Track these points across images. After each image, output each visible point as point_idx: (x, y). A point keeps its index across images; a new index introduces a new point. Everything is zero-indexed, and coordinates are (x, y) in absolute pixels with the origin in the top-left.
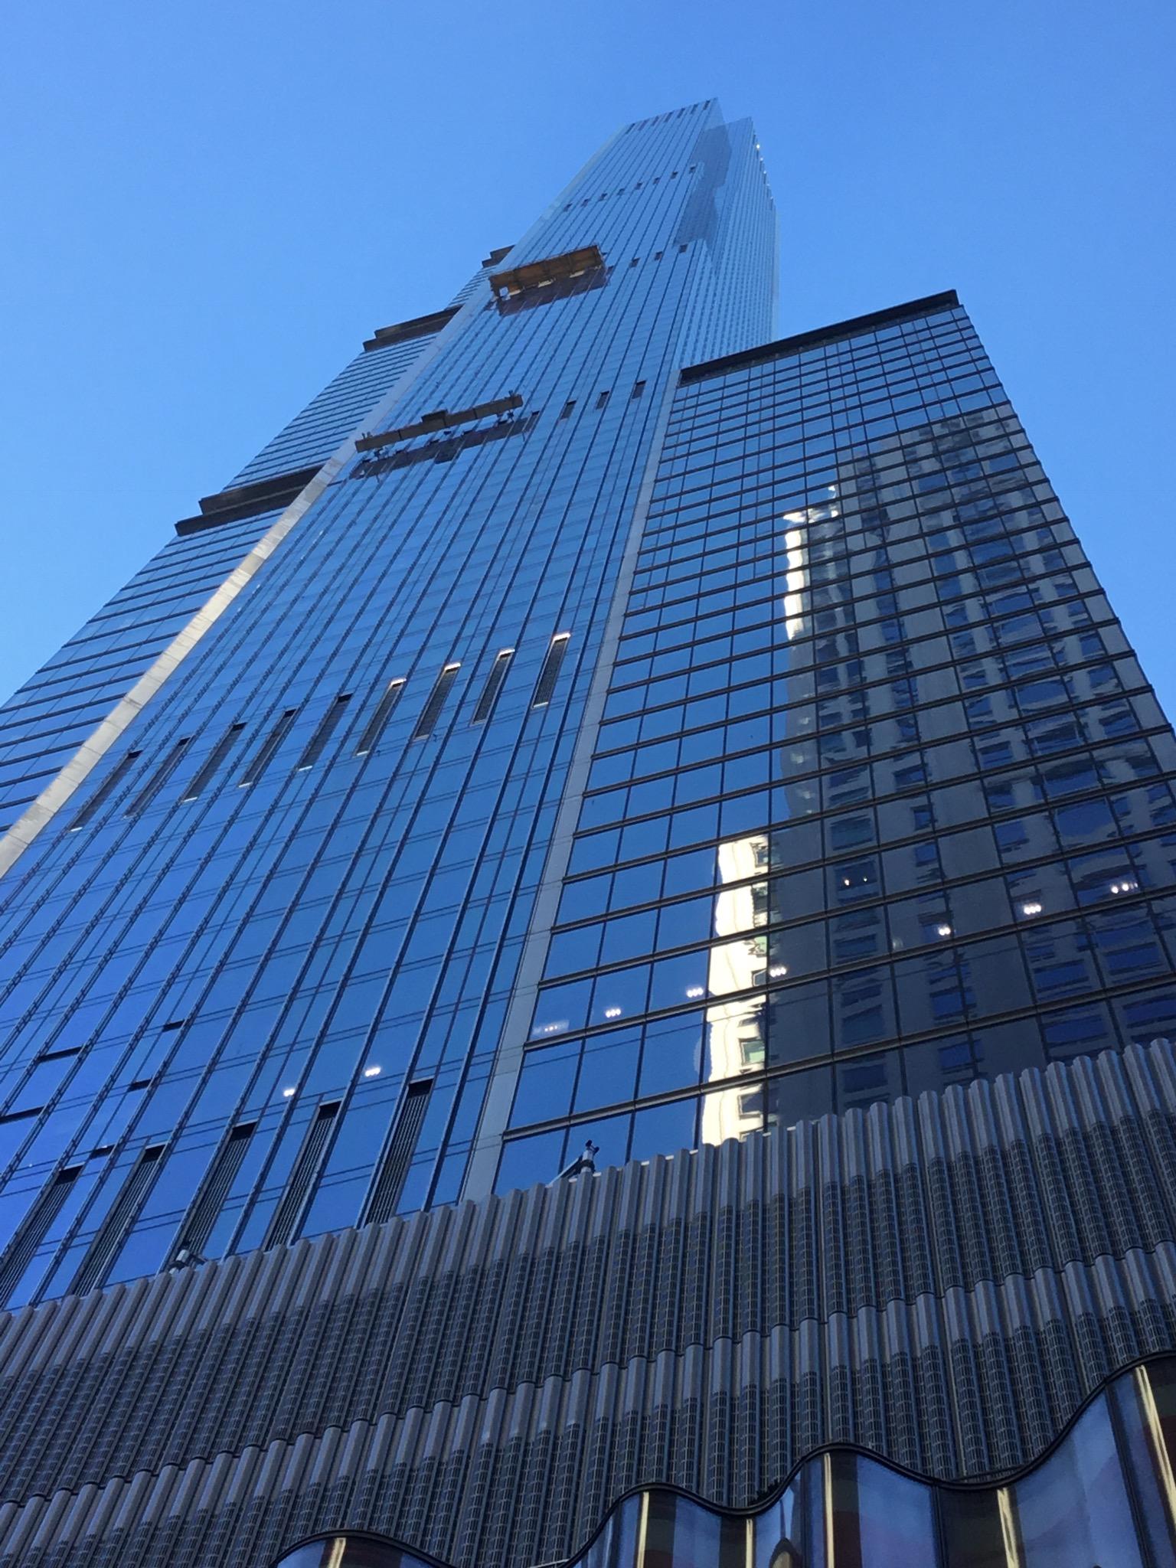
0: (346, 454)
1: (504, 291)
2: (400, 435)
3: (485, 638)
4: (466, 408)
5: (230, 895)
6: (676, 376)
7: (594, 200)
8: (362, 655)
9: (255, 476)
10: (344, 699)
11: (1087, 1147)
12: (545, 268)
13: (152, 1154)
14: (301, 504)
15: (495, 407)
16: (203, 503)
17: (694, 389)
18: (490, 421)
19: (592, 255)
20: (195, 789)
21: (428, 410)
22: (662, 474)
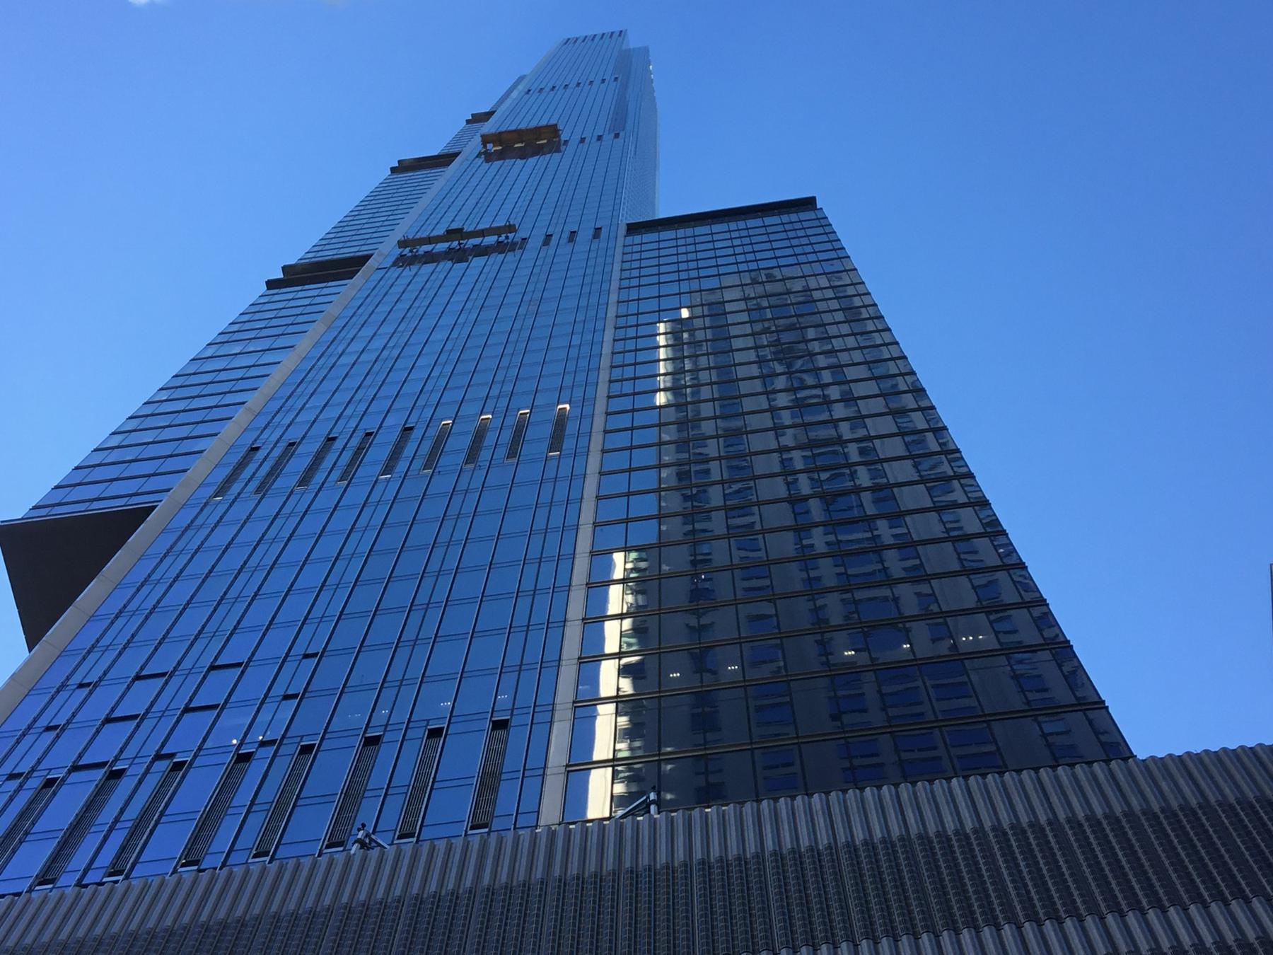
0: (387, 249)
1: (489, 146)
2: (429, 240)
4: (424, 235)
6: (623, 230)
7: (547, 89)
10: (407, 430)
12: (519, 134)
13: (50, 783)
16: (285, 269)
17: (637, 239)
19: (553, 130)
20: (305, 481)
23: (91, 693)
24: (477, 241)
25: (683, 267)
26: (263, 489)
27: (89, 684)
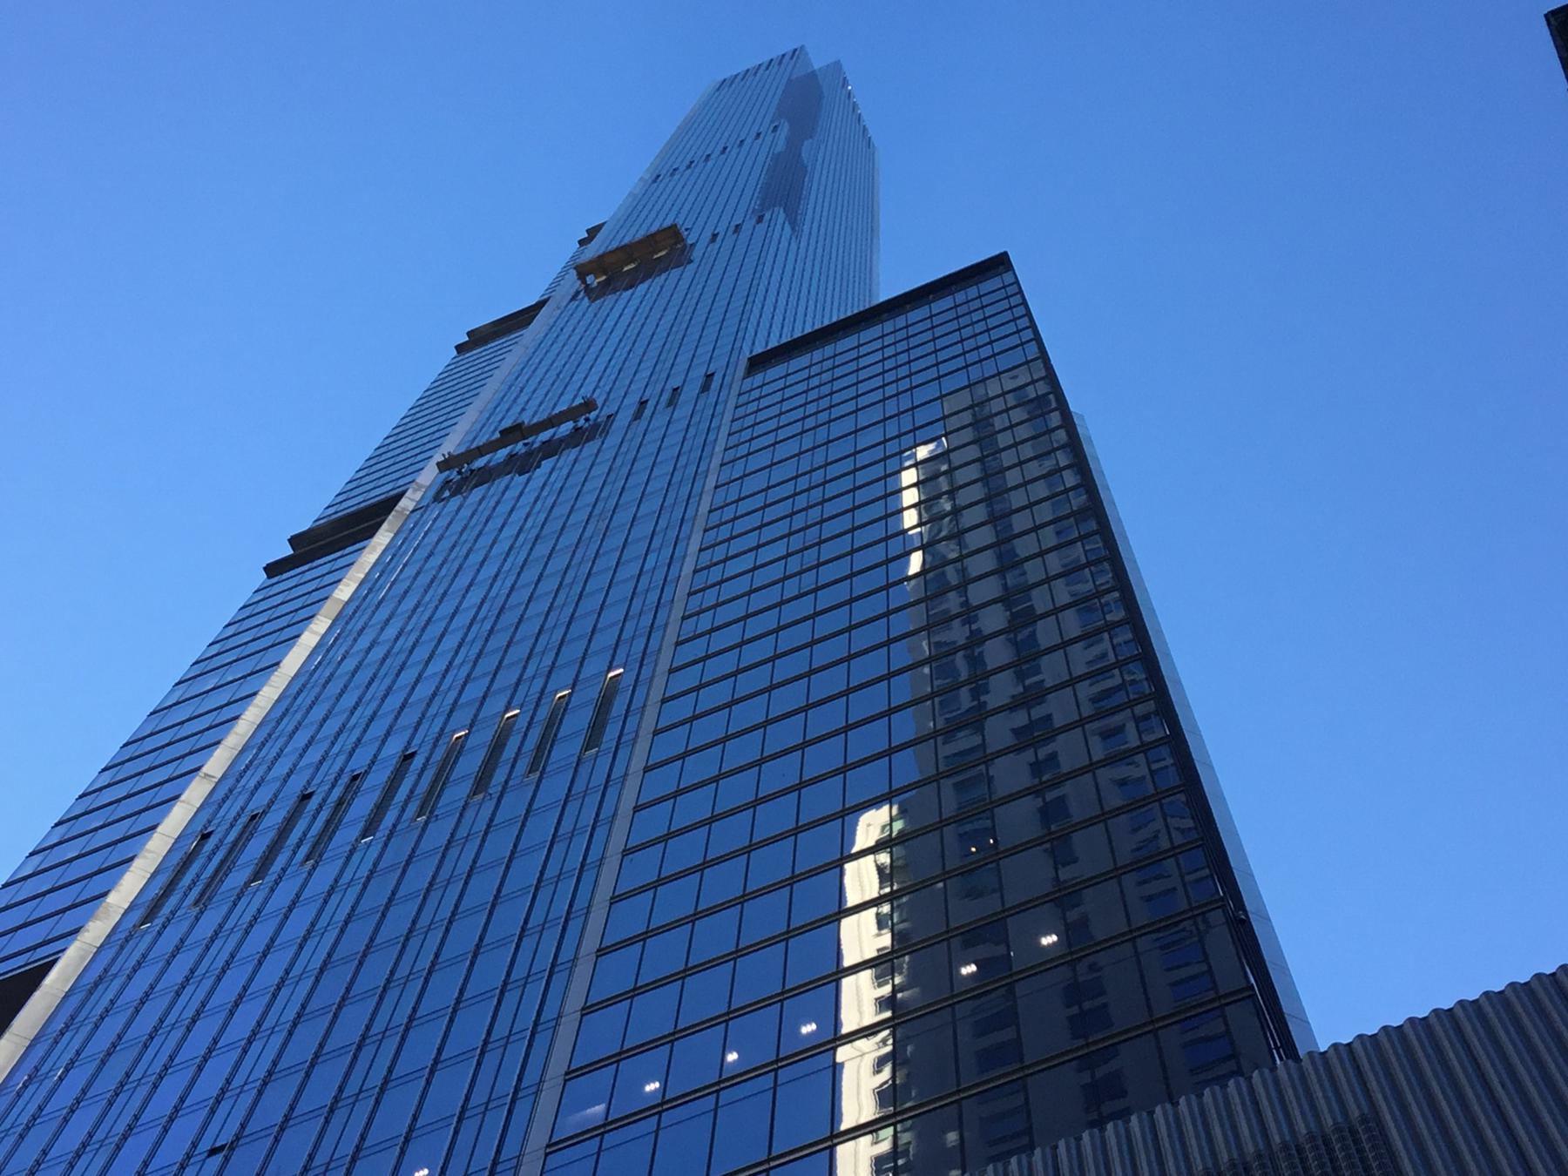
0: (429, 475)
2: (480, 451)
3: (644, 640)
4: (545, 416)
5: (414, 943)
6: (743, 364)
8: (428, 705)
9: (345, 505)
11: (1331, 1160)
12: (627, 251)
14: (383, 538)
15: (571, 414)
16: (293, 541)
17: (758, 379)
18: (566, 428)
19: (672, 235)
20: (258, 874)
21: (507, 423)
22: (722, 480)
23: (227, 1159)
24: (545, 436)
25: (969, 344)
26: (428, 805)
27: (222, 1148)
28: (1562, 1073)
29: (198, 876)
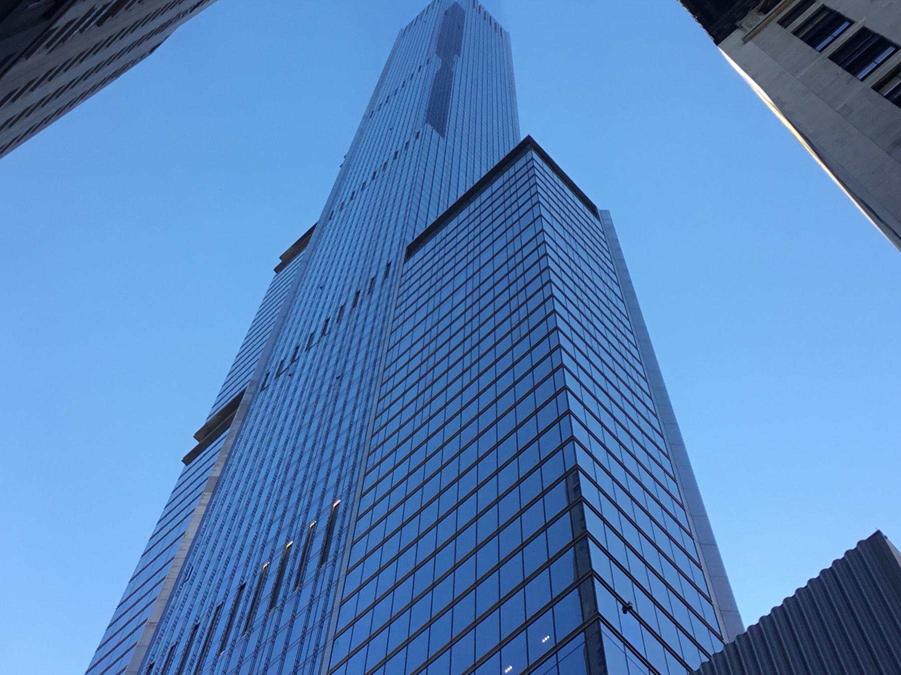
16: (197, 436)
20: (272, 604)
28: (897, 652)
29: (342, 527)
